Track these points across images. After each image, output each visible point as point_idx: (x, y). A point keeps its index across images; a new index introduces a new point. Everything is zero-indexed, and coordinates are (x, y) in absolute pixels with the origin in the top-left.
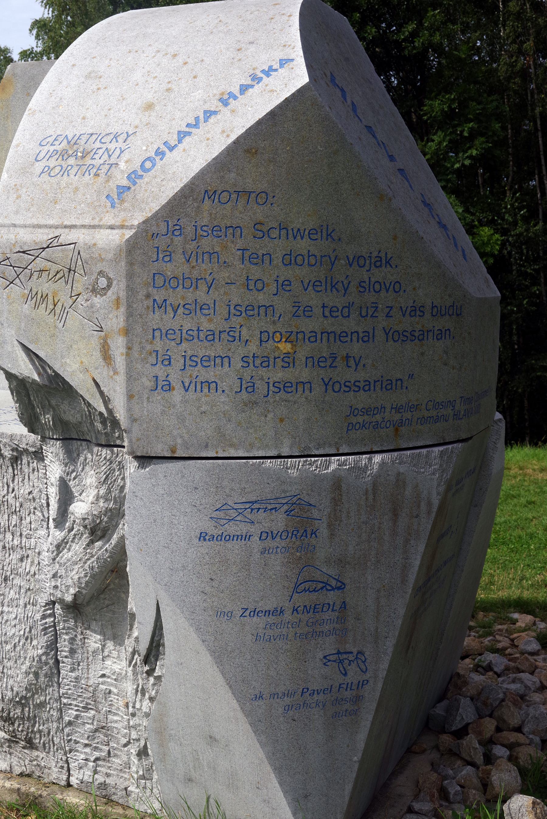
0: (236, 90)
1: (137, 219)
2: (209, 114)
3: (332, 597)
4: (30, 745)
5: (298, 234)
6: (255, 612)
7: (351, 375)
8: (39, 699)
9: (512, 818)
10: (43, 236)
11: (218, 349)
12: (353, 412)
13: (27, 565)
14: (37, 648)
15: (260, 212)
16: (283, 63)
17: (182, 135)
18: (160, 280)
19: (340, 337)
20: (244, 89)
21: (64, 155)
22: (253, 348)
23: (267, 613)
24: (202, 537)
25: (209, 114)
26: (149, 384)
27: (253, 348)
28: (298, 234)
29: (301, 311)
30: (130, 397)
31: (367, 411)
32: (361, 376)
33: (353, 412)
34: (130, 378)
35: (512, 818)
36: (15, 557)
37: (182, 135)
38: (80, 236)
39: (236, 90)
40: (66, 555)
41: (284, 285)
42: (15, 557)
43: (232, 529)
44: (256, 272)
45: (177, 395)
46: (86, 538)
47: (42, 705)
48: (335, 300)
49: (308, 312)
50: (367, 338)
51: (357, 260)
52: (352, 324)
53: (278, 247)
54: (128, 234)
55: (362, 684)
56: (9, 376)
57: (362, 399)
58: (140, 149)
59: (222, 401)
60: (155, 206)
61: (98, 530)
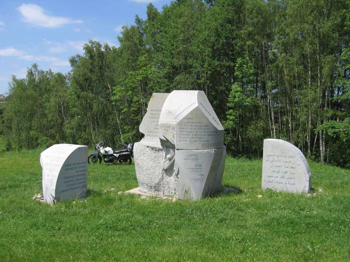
0: (189, 106)
1: (178, 121)
2: (11, 187)
3: (200, 167)
4: (158, 191)
5: (197, 123)
6: (191, 169)
7: (203, 140)
8: (160, 183)
9: (4, 188)
10: (166, 123)
11: (187, 136)
12: (203, 144)
13: (160, 165)
14: (160, 176)
15: (191, 121)
16: (195, 103)
17: (183, 111)
18: (180, 128)
19: (202, 135)
20: (191, 106)
21: (168, 112)
22: (191, 136)
23: (192, 169)
24: (185, 159)
25: (186, 109)
26: (179, 140)
27: (191, 136)
28: (197, 123)
29: (197, 132)
30: (176, 142)
31: (205, 144)
32: (204, 140)
33: (203, 144)
34: (176, 140)
35: (4, 188)
36: (158, 164)
37: (183, 111)
38: (171, 123)
39: (187, 108)
40: (166, 163)
41: (195, 129)
42: (158, 164)
43: (188, 158)
44: (192, 127)
45: (182, 142)
46: (168, 161)
47: (160, 184)
48: (201, 131)
49: (197, 132)
50: (205, 135)
51: (204, 126)
52: (203, 134)
53: (194, 124)
54: (177, 123)
55: (204, 179)
56: (160, 139)
57: (204, 143)
58: (178, 113)
59: (187, 142)
60: (180, 120)
61: (170, 159)
